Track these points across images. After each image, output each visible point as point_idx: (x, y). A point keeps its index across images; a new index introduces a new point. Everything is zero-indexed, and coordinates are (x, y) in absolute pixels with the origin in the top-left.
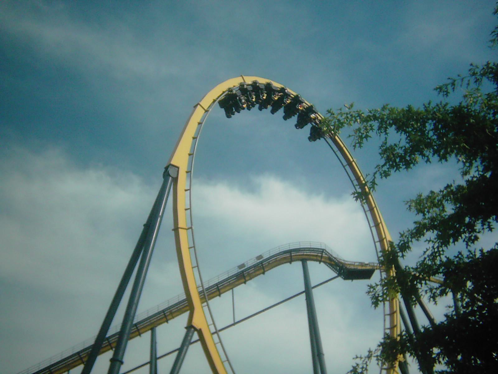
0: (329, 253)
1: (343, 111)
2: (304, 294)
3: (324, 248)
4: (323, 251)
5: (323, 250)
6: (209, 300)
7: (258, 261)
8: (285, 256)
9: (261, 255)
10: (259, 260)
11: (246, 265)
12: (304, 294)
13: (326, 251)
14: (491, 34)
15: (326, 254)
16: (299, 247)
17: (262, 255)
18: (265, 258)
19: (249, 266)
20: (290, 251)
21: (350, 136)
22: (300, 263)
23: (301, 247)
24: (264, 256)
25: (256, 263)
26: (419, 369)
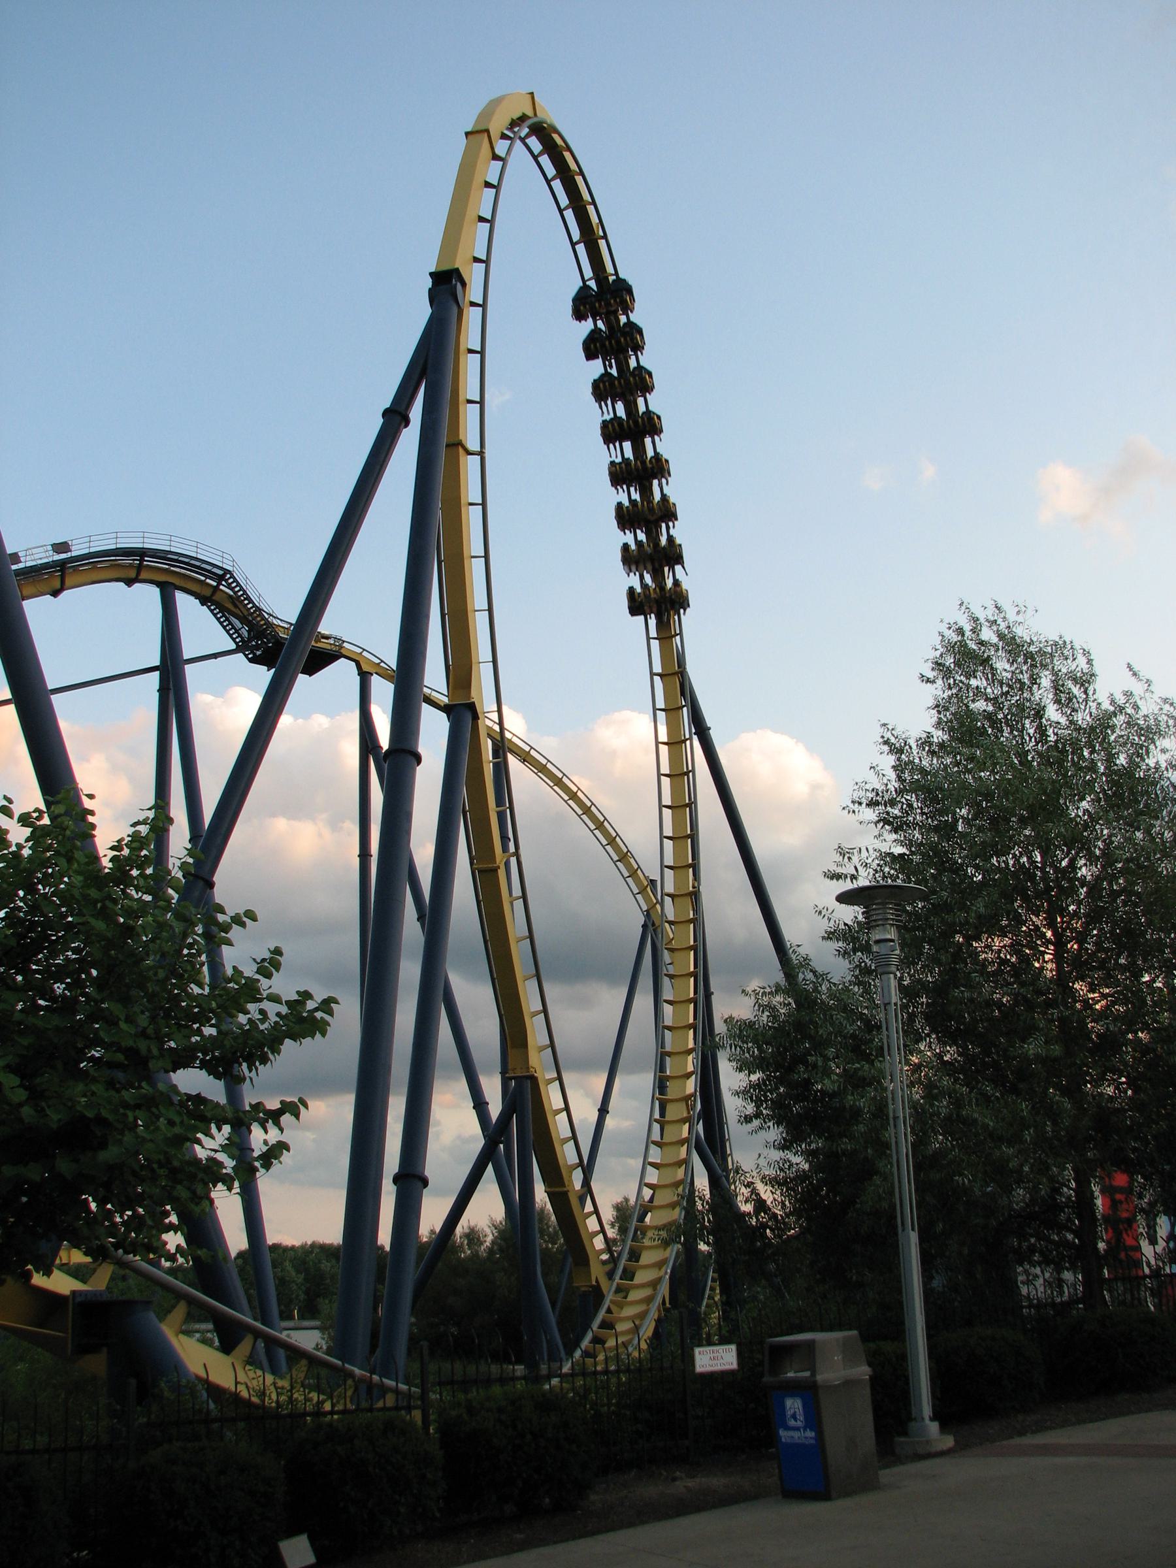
0: (238, 585)
1: (908, 741)
2: (156, 675)
3: (230, 568)
4: (224, 575)
5: (227, 571)
6: (302, 673)
7: (57, 557)
8: (127, 561)
9: (65, 544)
10: (59, 553)
11: (22, 559)
12: (156, 675)
13: (232, 576)
14: (618, 493)
15: (229, 586)
16: (140, 546)
17: (70, 543)
18: (74, 554)
19: (29, 564)
20: (142, 553)
21: (884, 725)
22: (154, 592)
23: (146, 546)
24: (73, 548)
25: (51, 559)
26: (797, 742)
